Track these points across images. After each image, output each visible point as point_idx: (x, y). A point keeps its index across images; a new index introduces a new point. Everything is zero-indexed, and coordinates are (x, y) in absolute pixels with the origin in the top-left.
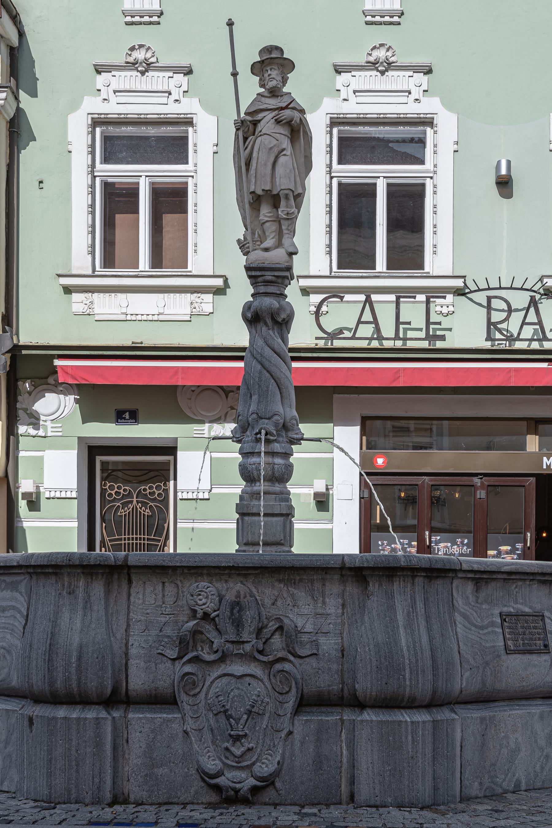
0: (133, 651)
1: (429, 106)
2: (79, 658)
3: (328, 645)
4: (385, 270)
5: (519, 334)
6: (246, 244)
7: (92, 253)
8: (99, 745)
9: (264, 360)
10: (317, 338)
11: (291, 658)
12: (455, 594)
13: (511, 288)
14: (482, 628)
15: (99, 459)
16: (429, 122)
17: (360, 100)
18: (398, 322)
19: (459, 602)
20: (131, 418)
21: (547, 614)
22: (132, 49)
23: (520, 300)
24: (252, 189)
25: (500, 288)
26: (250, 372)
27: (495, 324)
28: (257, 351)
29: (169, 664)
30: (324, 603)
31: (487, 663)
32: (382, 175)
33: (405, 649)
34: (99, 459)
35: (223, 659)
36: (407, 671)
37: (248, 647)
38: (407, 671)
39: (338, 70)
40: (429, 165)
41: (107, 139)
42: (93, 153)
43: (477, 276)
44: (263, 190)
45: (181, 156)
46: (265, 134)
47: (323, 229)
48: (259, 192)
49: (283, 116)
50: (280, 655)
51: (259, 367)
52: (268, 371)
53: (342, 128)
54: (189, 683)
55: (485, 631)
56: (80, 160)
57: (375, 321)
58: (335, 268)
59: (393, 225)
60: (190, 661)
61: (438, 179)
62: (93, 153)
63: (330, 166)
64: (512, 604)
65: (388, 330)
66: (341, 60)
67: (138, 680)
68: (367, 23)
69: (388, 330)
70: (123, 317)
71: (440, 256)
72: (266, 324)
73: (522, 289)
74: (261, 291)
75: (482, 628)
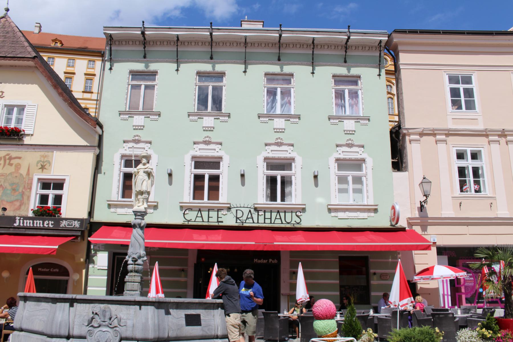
0: (76, 323)
1: (293, 155)
2: (60, 325)
3: (130, 323)
4: (191, 200)
7: (118, 194)
11: (119, 326)
14: (178, 318)
15: (116, 256)
16: (364, 160)
18: (209, 217)
22: (205, 137)
23: (246, 211)
27: (238, 218)
29: (85, 327)
32: (207, 173)
34: (116, 256)
35: (99, 326)
37: (107, 323)
39: (266, 145)
40: (364, 172)
41: (196, 163)
42: (121, 165)
43: (234, 204)
45: (218, 168)
47: (188, 188)
50: (115, 325)
54: (90, 333)
56: (117, 167)
57: (202, 217)
59: (210, 188)
60: (91, 326)
61: (368, 177)
62: (121, 165)
63: (191, 170)
65: (206, 219)
66: (126, 139)
67: (76, 332)
68: (275, 132)
69: (206, 219)
71: (224, 197)
75: (178, 318)
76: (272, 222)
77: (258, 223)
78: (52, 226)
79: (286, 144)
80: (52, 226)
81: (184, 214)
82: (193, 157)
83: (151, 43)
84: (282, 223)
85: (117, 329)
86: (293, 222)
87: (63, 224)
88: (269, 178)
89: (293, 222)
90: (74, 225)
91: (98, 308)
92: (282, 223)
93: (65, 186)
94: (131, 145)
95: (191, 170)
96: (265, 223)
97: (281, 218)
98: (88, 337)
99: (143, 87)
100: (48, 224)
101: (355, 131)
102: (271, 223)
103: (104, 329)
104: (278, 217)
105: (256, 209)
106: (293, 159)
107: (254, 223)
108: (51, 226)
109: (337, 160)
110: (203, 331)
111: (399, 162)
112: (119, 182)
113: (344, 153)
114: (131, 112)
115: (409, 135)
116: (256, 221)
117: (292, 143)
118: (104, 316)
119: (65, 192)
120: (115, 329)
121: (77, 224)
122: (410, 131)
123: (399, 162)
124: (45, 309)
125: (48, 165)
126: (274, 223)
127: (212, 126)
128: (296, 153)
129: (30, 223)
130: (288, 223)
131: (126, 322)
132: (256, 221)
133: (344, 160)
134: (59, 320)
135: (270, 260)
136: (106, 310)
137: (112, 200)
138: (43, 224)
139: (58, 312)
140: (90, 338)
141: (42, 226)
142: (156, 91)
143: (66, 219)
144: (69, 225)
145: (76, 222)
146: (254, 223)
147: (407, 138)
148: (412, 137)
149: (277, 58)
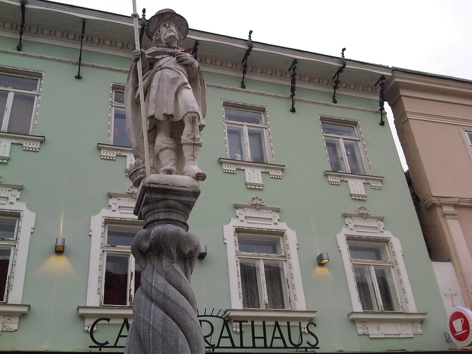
5: (219, 344)
6: (141, 169)
9: (168, 302)
10: (90, 347)
13: (211, 316)
17: (122, 211)
20: (50, 34)
24: (150, 114)
25: (205, 316)
26: (147, 320)
28: (157, 290)
44: (165, 115)
46: (166, 68)
48: (160, 116)
49: (185, 56)
51: (162, 313)
52: (173, 319)
53: (110, 225)
58: (103, 304)
66: (112, 191)
72: (170, 257)
73: (217, 316)
74: (161, 218)
76: (269, 345)
77: (242, 347)
79: (268, 209)
82: (108, 222)
83: (34, 30)
84: (286, 347)
86: (304, 344)
88: (127, 256)
89: (304, 344)
92: (286, 347)
94: (249, 213)
96: (254, 347)
97: (282, 337)
99: (11, 97)
101: (365, 196)
102: (266, 347)
104: (277, 334)
106: (17, 215)
107: (234, 347)
109: (238, 231)
111: (436, 249)
113: (245, 219)
114: (235, 162)
115: (441, 206)
116: (237, 344)
117: (382, 216)
122: (442, 200)
123: (436, 249)
126: (271, 347)
127: (7, 155)
128: (285, 224)
130: (297, 347)
132: (237, 344)
133: (359, 239)
142: (36, 105)
146: (234, 347)
147: (439, 211)
148: (446, 209)
149: (240, 85)
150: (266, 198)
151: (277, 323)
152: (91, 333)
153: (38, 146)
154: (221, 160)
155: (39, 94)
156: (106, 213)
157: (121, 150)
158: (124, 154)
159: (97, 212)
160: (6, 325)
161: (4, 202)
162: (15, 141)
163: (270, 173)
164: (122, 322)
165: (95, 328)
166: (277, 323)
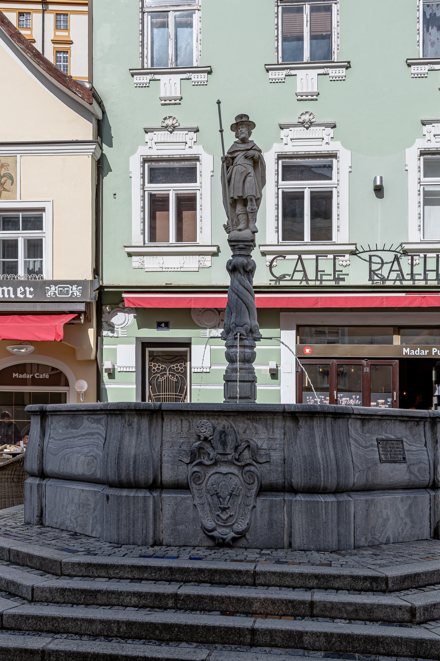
0: (165, 459)
2: (135, 462)
3: (276, 456)
5: (388, 277)
8: (145, 512)
10: (270, 280)
12: (350, 428)
13: (383, 250)
14: (366, 447)
15: (147, 350)
17: (294, 144)
19: (352, 432)
21: (404, 440)
23: (389, 257)
25: (377, 250)
27: (374, 271)
29: (185, 466)
30: (273, 432)
31: (369, 468)
33: (320, 459)
34: (147, 350)
35: (216, 463)
36: (322, 472)
37: (230, 457)
38: (322, 472)
42: (143, 178)
43: (363, 243)
50: (248, 462)
53: (284, 160)
55: (368, 449)
56: (136, 181)
57: (304, 270)
60: (197, 465)
62: (143, 178)
63: (277, 182)
64: (384, 434)
66: (283, 121)
67: (168, 475)
70: (161, 270)
71: (341, 234)
73: (389, 251)
75: (366, 447)
78: (31, 297)
80: (31, 297)
81: (271, 266)
85: (252, 468)
87: (52, 292)
90: (71, 292)
91: (205, 426)
93: (47, 218)
95: (277, 182)
98: (193, 486)
100: (24, 293)
103: (224, 469)
105: (405, 253)
108: (28, 296)
110: (411, 473)
112: (144, 211)
114: (154, 70)
118: (224, 444)
119: (47, 235)
120: (247, 468)
121: (76, 292)
124: (92, 434)
125: (9, 181)
129: (9, 291)
131: (269, 456)
134: (133, 452)
135: (434, 350)
136: (227, 431)
137: (133, 244)
138: (15, 293)
139: (127, 438)
140: (198, 487)
141: (12, 296)
143: (56, 283)
144: (61, 292)
145: (74, 288)
150: (320, 112)
151: (300, 258)
152: (271, 266)
153: (344, 74)
154: (408, 61)
155: (199, 8)
156: (421, 144)
157: (291, 69)
158: (293, 72)
159: (133, 152)
160: (201, 262)
161: (320, 143)
162: (321, 71)
163: (331, 75)
164: (296, 257)
165: (274, 263)
166: (300, 258)
